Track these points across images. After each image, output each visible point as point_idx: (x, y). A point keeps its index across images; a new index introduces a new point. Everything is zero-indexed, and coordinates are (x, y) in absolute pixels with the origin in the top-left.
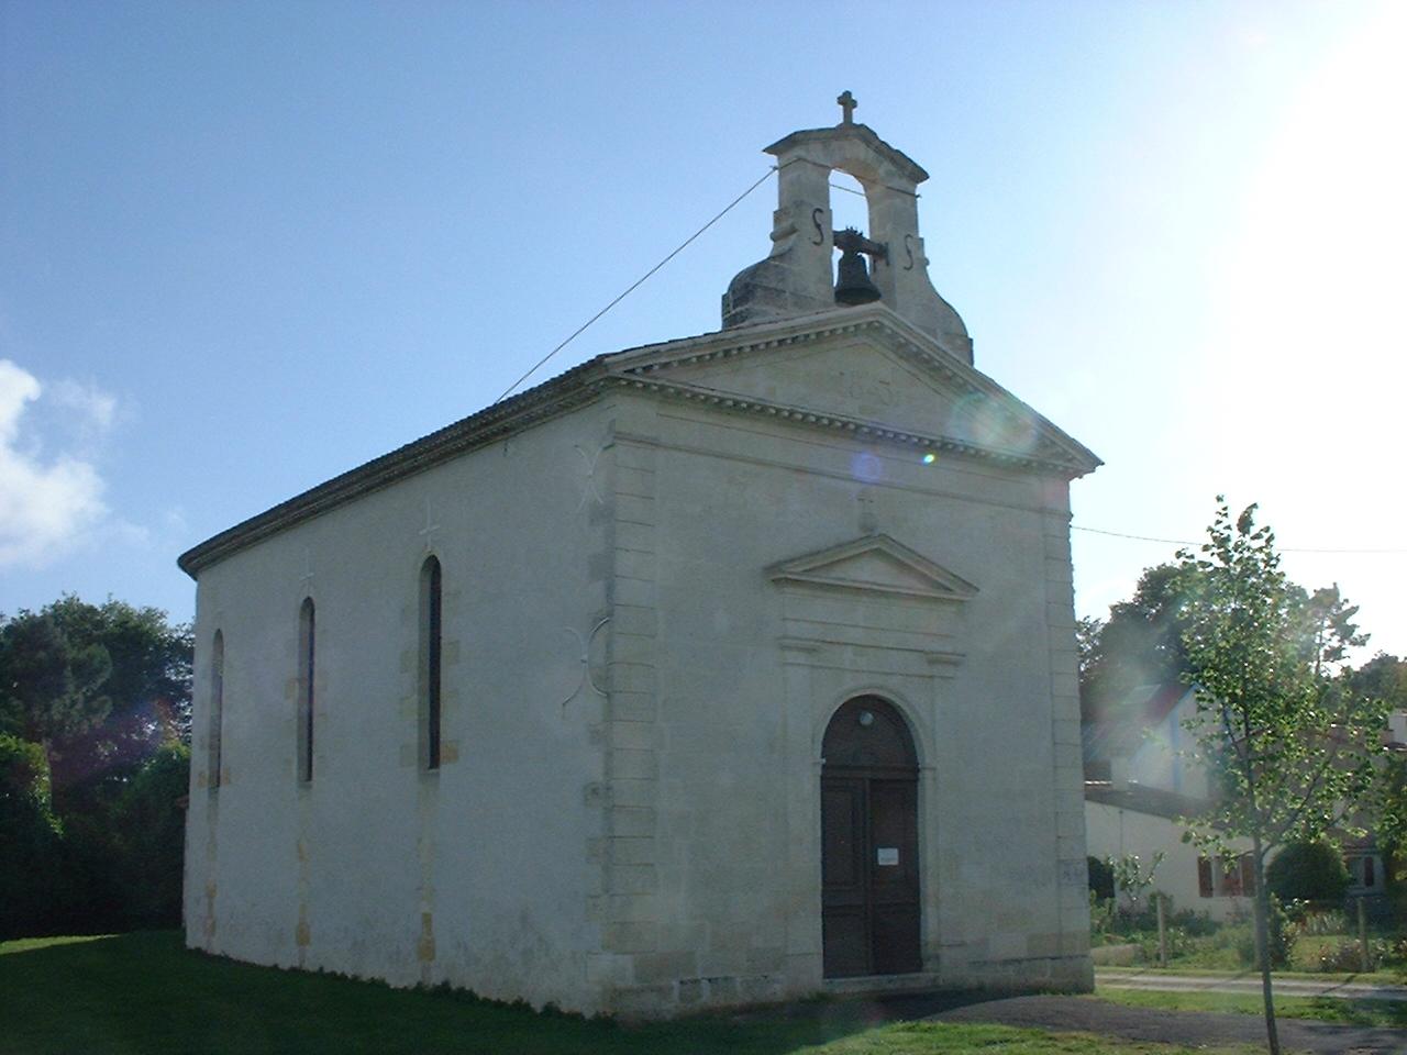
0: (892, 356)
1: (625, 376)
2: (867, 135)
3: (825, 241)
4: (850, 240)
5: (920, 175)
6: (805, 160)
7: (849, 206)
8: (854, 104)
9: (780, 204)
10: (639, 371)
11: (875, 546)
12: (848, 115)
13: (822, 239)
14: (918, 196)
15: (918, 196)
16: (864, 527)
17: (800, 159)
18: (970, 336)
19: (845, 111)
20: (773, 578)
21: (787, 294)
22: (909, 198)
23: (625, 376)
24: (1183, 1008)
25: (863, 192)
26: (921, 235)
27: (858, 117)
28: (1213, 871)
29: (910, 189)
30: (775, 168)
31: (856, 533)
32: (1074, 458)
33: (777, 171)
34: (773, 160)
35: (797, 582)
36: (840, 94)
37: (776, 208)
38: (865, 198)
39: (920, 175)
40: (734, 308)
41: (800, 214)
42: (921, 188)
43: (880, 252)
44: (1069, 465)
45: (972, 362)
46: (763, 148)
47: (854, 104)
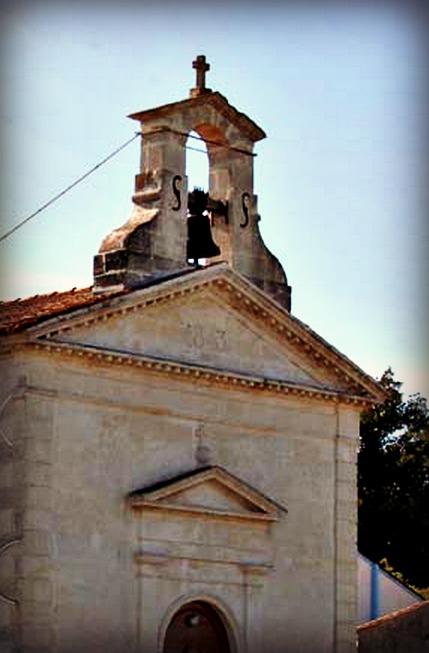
0: (227, 307)
1: (39, 342)
2: (219, 101)
3: (182, 205)
4: (198, 199)
5: (257, 134)
6: (169, 130)
7: (199, 170)
8: (207, 67)
9: (142, 167)
10: (48, 336)
11: (211, 476)
12: (201, 80)
13: (180, 205)
14: (255, 155)
15: (255, 155)
16: (200, 461)
17: (166, 130)
18: (289, 284)
19: (204, 84)
20: (134, 504)
21: (152, 258)
22: (246, 157)
23: (39, 342)
24: (47, 358)
25: (206, 150)
26: (255, 193)
27: (212, 82)
28: (251, 500)
29: (249, 147)
30: (139, 134)
31: (193, 464)
32: (367, 393)
33: (140, 137)
34: (137, 126)
35: (152, 509)
36: (195, 59)
37: (138, 172)
38: (206, 155)
39: (257, 134)
40: (107, 271)
41: (159, 180)
42: (258, 147)
43: (222, 210)
44: (363, 399)
45: (289, 310)
46: (128, 114)
47: (207, 67)
